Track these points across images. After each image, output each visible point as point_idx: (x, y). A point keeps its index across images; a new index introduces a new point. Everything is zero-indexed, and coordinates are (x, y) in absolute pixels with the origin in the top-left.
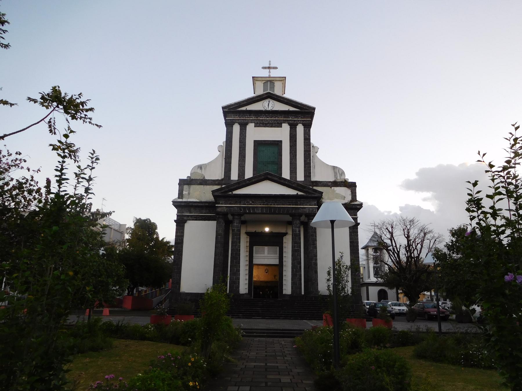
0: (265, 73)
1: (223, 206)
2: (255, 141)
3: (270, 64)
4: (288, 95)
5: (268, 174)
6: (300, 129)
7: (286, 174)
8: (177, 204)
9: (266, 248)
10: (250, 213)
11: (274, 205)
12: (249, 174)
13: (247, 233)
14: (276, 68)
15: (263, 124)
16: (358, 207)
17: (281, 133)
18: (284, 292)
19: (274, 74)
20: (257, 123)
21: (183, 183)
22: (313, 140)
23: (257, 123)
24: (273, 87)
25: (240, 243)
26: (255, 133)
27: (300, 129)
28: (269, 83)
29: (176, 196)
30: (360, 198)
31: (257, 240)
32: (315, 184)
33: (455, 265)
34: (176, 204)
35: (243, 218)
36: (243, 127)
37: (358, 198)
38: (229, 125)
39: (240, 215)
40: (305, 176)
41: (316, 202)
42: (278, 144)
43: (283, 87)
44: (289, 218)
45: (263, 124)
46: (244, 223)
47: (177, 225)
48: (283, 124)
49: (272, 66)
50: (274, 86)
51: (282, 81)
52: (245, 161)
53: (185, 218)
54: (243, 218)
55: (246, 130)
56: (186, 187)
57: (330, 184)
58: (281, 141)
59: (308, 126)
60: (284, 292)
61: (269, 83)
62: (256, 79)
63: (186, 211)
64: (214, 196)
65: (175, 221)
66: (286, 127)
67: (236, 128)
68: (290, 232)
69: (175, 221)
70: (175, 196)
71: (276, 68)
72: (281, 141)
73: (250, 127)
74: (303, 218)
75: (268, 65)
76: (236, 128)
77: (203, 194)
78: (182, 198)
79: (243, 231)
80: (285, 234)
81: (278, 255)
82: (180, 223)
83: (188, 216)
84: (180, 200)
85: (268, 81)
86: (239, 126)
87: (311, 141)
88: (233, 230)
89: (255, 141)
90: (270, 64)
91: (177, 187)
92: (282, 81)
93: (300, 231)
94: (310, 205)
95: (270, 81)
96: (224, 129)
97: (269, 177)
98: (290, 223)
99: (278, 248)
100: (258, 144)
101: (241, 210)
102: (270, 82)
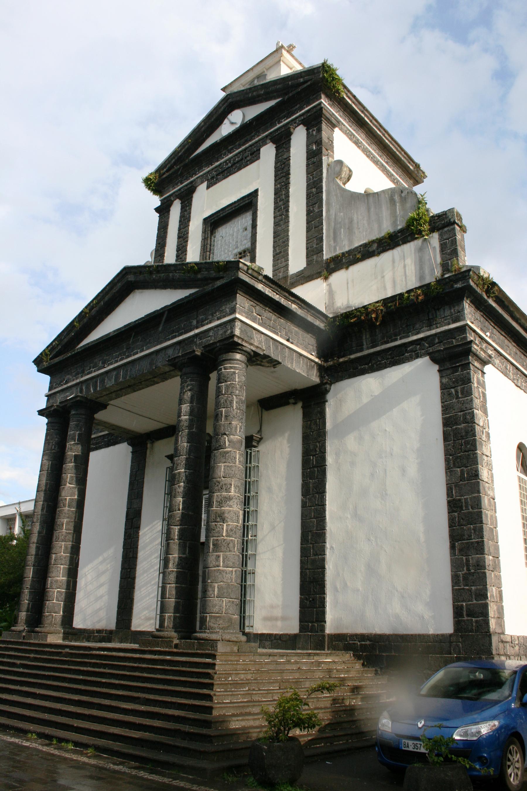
20: (213, 178)
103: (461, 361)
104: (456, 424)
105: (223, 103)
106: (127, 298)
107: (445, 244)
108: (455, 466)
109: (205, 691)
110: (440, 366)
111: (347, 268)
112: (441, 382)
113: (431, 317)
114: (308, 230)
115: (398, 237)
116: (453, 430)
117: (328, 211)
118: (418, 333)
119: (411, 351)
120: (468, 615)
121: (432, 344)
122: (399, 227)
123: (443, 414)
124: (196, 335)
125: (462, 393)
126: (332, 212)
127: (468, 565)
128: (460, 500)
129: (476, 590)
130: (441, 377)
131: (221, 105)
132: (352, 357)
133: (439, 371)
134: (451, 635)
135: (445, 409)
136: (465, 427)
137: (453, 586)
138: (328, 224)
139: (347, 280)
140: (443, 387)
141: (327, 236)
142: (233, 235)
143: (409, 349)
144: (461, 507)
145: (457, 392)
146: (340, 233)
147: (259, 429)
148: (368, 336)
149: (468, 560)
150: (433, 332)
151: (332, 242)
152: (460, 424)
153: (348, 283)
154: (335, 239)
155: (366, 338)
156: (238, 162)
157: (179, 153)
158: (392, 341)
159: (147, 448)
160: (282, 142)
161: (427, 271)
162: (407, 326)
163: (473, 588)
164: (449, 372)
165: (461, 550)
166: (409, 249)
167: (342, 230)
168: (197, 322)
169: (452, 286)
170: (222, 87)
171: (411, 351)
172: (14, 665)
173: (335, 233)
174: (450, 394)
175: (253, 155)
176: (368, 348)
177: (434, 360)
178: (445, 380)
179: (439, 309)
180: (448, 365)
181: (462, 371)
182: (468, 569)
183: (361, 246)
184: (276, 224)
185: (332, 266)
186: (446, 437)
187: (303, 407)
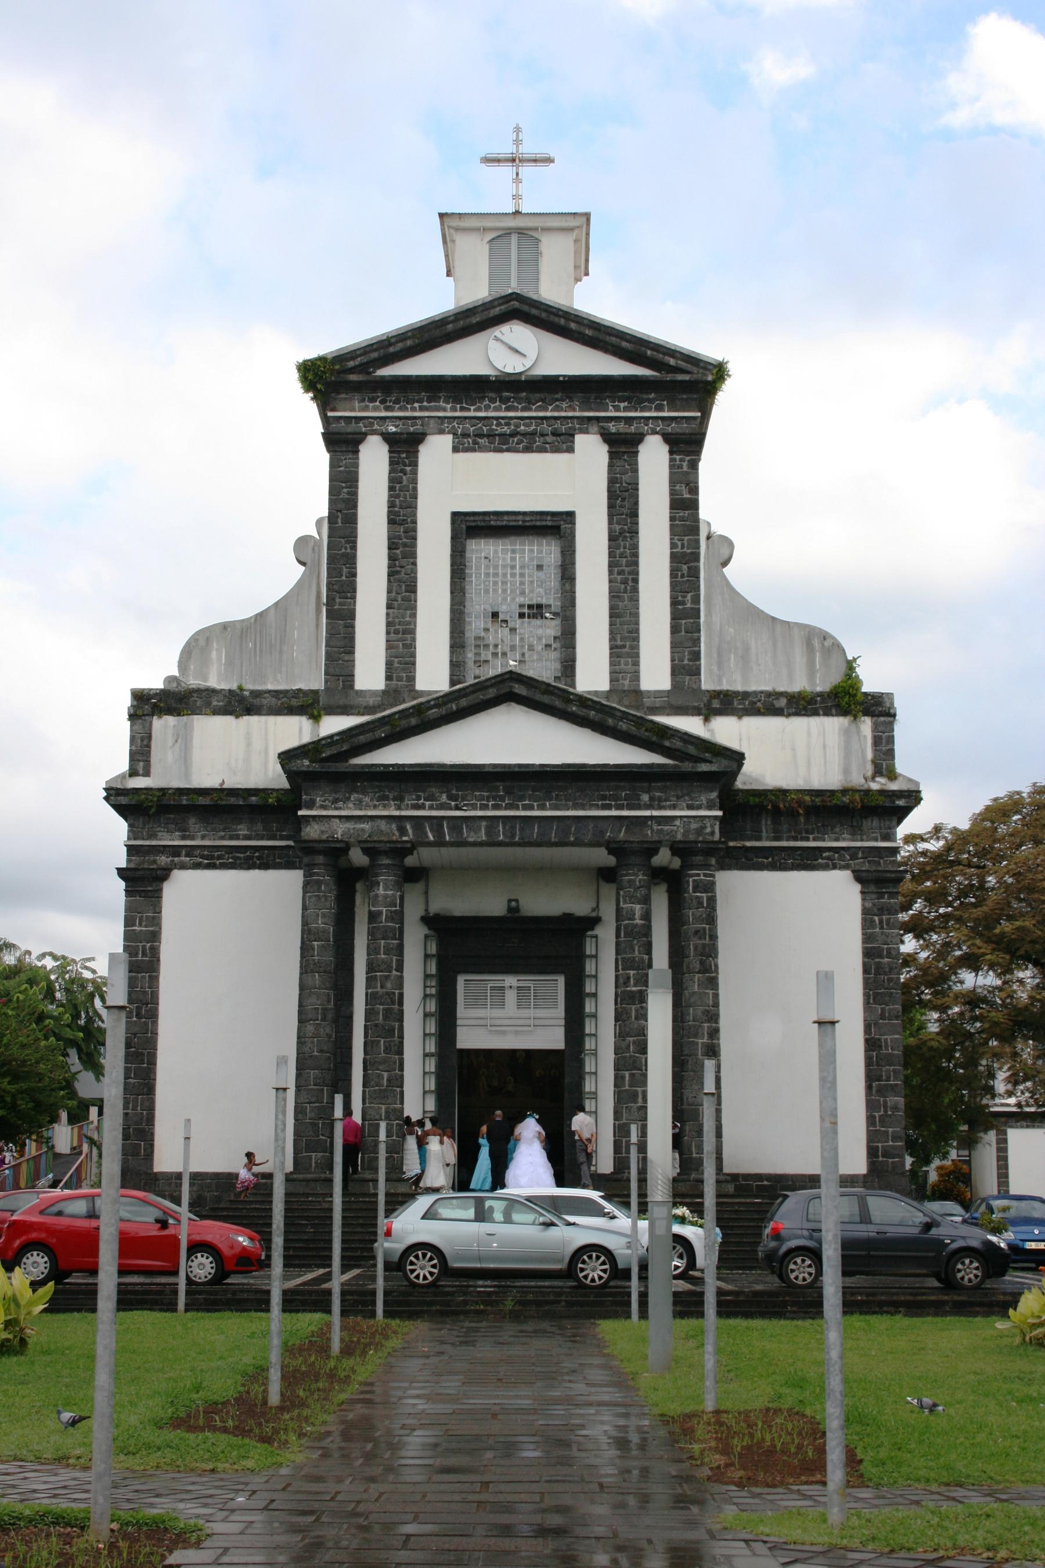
0: (493, 194)
1: (332, 817)
2: (456, 516)
3: (517, 142)
4: (595, 299)
5: (512, 676)
6: (653, 459)
7: (593, 676)
8: (123, 800)
9: (511, 980)
10: (440, 843)
11: (542, 807)
12: (433, 675)
13: (428, 920)
14: (549, 160)
15: (490, 436)
16: (901, 803)
17: (572, 479)
18: (341, 1096)
19: (543, 194)
20: (465, 435)
21: (146, 706)
22: (712, 511)
23: (465, 435)
24: (531, 262)
25: (400, 967)
26: (456, 479)
27: (653, 459)
28: (514, 238)
29: (123, 765)
30: (907, 763)
31: (468, 948)
32: (716, 704)
33: (234, 1186)
34: (122, 799)
35: (410, 861)
36: (404, 448)
37: (901, 766)
38: (342, 443)
39: (400, 851)
40: (676, 671)
41: (714, 795)
42: (556, 527)
43: (577, 253)
44: (602, 857)
45: (490, 436)
46: (414, 875)
47: (128, 892)
48: (579, 439)
49: (528, 148)
50: (538, 254)
51: (571, 229)
52: (413, 608)
53: (163, 860)
54: (410, 861)
55: (415, 464)
56: (163, 726)
57: (783, 702)
58: (570, 516)
59: (687, 445)
60: (341, 1096)
61: (514, 238)
62: (455, 223)
63: (168, 826)
64: (291, 775)
65: (121, 873)
66: (591, 452)
67: (374, 460)
68: (608, 912)
69: (121, 873)
70: (116, 761)
71: (549, 160)
72: (570, 516)
73: (436, 453)
74: (663, 857)
75: (506, 148)
76: (374, 460)
77: (238, 754)
78: (147, 773)
79: (413, 911)
80: (594, 921)
81: (560, 1011)
82: (143, 881)
83: (175, 851)
84: (139, 782)
85: (508, 232)
86: (384, 449)
87: (703, 514)
88: (373, 917)
89: (456, 516)
90: (517, 142)
91: (123, 729)
92: (571, 229)
93: (647, 916)
94: (690, 807)
95: (521, 232)
96: (322, 458)
97: (520, 689)
98: (607, 875)
99: (561, 980)
100: (470, 527)
101: (402, 831)
102: (516, 234)
103: (888, 888)
104: (881, 956)
105: (501, 301)
106: (493, 709)
107: (880, 737)
108: (875, 1003)
109: (348, 1254)
110: (863, 887)
111: (740, 717)
112: (863, 905)
113: (855, 824)
114: (675, 630)
115: (816, 702)
116: (876, 963)
117: (709, 614)
118: (837, 840)
119: (828, 858)
120: (883, 1156)
121: (853, 857)
122: (819, 689)
123: (863, 943)
124: (652, 818)
125: (888, 924)
126: (716, 619)
127: (885, 1107)
128: (879, 1040)
129: (893, 1132)
130: (863, 899)
131: (496, 303)
132: (748, 844)
133: (862, 892)
134: (864, 1176)
135: (867, 938)
136: (889, 963)
137: (868, 1127)
138: (709, 636)
139: (740, 734)
140: (866, 912)
141: (706, 655)
142: (513, 567)
143: (824, 855)
144: (880, 1047)
145: (881, 922)
146: (729, 659)
147: (594, 905)
148: (769, 823)
149: (885, 1102)
150: (859, 844)
151: (715, 668)
152: (883, 958)
153: (740, 740)
154: (720, 664)
155: (766, 824)
156: (524, 435)
157: (390, 345)
158: (803, 839)
159: (354, 891)
160: (623, 448)
161: (854, 768)
162: (823, 825)
163: (890, 1130)
164: (874, 896)
165: (879, 1091)
166: (832, 726)
167: (732, 656)
168: (652, 799)
169: (894, 802)
170: (443, 211)
171: (828, 858)
172: (362, 1225)
173: (719, 655)
174: (872, 921)
175: (561, 441)
176: (768, 839)
177: (859, 878)
178: (868, 905)
179: (866, 818)
180: (872, 888)
181: (889, 898)
182: (886, 1111)
183: (761, 692)
184: (614, 595)
185: (716, 704)
186: (866, 970)
187: (669, 891)
